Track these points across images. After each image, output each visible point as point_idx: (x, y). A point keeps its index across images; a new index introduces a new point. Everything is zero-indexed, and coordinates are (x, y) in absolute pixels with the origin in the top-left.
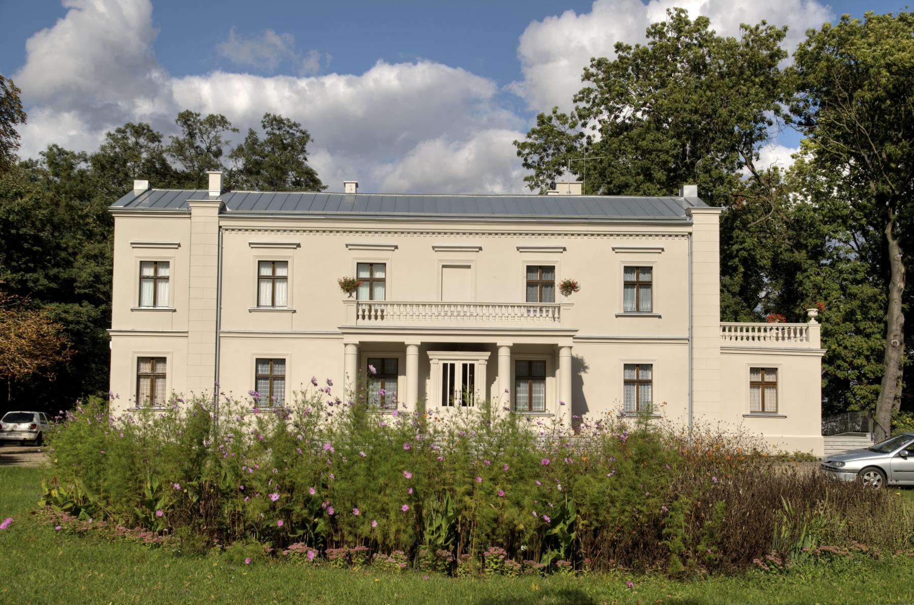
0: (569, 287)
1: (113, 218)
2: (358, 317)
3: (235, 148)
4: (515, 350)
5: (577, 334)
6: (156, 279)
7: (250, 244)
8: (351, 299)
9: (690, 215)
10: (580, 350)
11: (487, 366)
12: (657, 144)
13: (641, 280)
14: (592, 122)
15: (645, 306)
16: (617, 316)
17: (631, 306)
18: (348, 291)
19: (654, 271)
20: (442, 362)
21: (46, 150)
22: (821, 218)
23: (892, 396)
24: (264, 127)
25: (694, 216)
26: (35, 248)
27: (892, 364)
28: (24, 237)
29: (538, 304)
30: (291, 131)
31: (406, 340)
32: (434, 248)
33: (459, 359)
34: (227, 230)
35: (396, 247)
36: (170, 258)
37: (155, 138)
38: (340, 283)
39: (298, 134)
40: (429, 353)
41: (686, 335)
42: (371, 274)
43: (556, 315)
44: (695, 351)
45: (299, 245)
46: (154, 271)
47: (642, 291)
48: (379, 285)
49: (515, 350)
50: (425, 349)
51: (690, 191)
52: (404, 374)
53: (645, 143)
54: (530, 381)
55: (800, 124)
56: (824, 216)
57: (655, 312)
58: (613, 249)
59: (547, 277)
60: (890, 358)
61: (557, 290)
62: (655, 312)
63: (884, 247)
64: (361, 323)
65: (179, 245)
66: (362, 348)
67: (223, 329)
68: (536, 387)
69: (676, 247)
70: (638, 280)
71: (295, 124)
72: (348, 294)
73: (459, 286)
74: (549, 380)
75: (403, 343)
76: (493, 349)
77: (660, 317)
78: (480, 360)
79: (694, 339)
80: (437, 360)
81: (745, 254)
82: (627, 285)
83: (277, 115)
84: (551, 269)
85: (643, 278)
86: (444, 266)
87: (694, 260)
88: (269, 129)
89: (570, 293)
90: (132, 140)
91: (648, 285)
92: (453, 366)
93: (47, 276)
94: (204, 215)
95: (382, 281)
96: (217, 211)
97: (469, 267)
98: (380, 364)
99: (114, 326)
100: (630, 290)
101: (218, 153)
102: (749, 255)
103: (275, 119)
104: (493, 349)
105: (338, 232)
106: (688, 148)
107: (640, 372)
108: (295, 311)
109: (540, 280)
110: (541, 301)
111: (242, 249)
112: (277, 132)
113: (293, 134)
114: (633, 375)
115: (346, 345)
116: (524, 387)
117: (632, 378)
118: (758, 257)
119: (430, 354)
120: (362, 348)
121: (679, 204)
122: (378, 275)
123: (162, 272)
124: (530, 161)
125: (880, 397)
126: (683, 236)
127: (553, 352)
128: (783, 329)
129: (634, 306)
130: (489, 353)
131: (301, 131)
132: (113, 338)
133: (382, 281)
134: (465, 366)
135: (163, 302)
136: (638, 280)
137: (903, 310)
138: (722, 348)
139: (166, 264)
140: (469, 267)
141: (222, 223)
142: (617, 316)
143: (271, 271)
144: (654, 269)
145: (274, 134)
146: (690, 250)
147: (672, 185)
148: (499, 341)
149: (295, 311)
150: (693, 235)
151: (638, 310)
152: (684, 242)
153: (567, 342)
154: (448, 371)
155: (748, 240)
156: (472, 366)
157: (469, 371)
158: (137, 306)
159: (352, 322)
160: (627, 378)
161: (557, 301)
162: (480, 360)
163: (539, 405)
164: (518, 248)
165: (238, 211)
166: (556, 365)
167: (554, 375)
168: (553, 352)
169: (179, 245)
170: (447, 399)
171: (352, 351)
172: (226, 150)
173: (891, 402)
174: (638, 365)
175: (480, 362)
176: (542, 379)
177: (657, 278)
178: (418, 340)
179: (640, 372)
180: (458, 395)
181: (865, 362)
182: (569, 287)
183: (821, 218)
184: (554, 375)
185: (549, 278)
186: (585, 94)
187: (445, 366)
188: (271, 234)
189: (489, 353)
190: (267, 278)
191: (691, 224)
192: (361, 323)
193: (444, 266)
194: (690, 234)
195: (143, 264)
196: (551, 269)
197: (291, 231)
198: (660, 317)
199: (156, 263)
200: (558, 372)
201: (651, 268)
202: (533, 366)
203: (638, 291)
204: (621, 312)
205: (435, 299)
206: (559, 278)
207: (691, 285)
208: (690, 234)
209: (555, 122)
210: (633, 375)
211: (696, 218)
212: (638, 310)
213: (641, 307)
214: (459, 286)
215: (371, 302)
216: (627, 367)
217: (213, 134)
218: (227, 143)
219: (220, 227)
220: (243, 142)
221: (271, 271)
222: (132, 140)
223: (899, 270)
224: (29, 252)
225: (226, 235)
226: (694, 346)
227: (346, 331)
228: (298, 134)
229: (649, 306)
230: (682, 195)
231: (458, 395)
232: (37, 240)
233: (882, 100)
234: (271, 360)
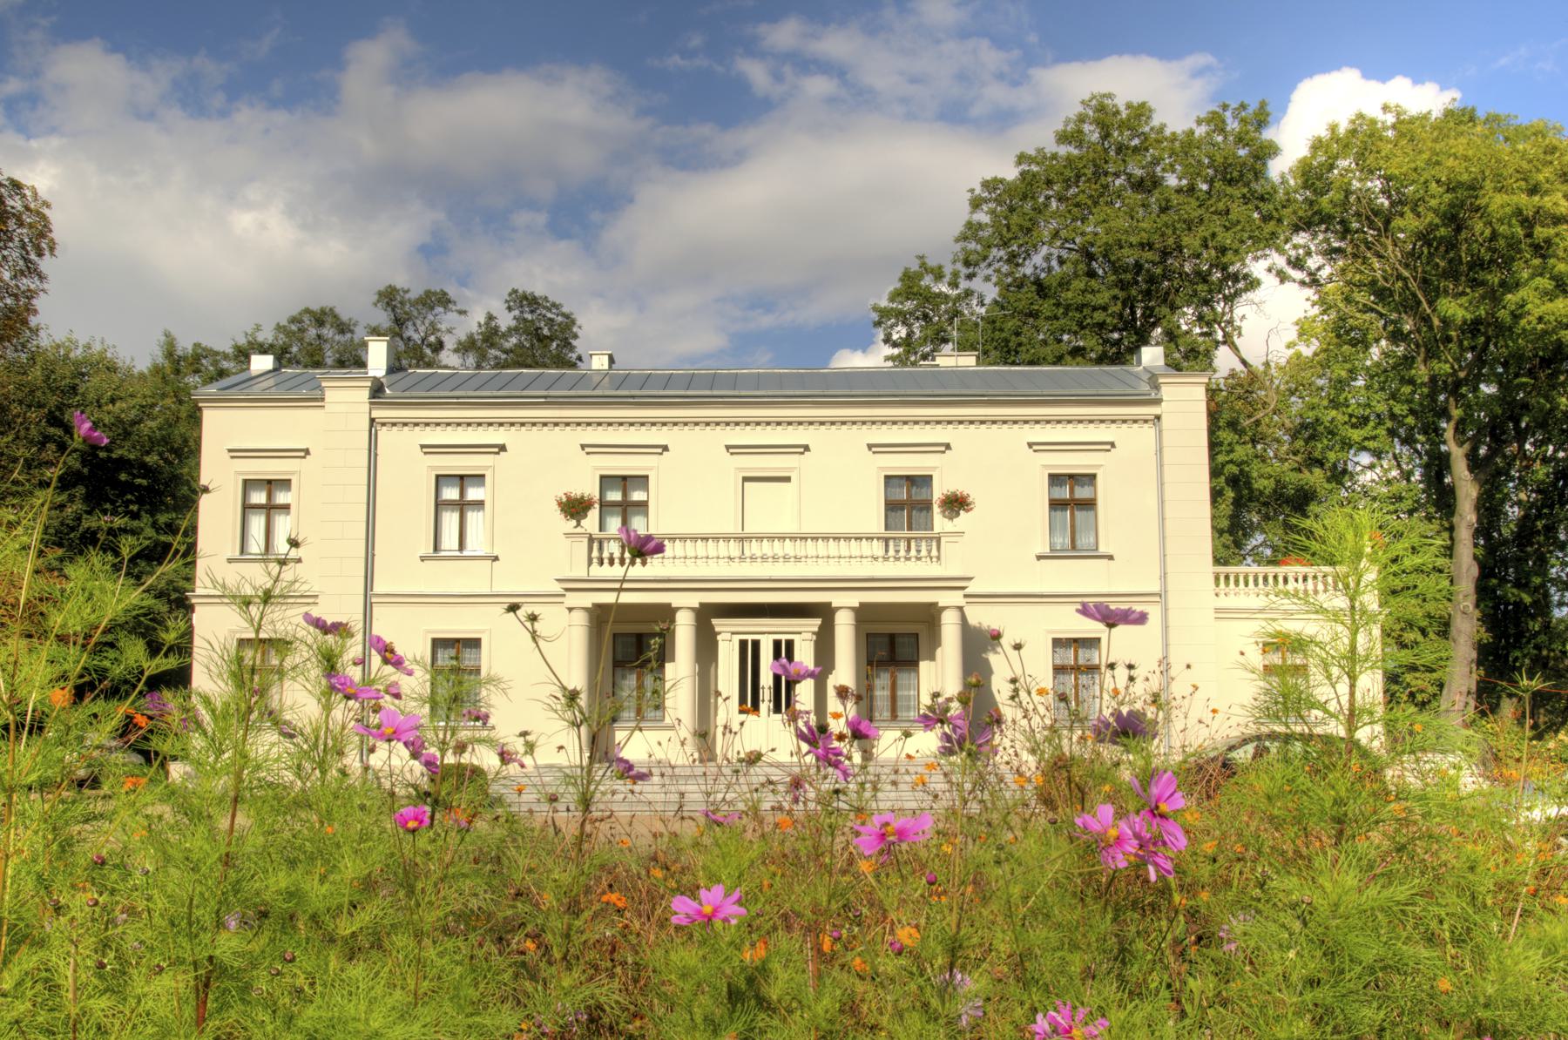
0: (956, 504)
1: (200, 409)
2: (590, 562)
3: (463, 338)
4: (864, 614)
5: (973, 588)
6: (462, 506)
7: (422, 446)
8: (579, 530)
9: (1157, 387)
10: (981, 616)
11: (817, 644)
12: (1089, 296)
13: (1077, 496)
14: (983, 271)
15: (1084, 540)
16: (1039, 558)
17: (1063, 540)
18: (572, 517)
19: (1100, 480)
20: (737, 638)
21: (185, 345)
22: (1346, 418)
23: (1464, 689)
24: (510, 309)
25: (1164, 389)
26: (138, 481)
27: (1462, 640)
28: (123, 463)
29: (906, 533)
30: (549, 315)
31: (674, 599)
32: (728, 447)
33: (766, 632)
34: (383, 424)
35: (665, 448)
36: (292, 473)
37: (343, 328)
38: (560, 503)
39: (560, 319)
40: (714, 621)
41: (1156, 588)
42: (625, 494)
43: (934, 553)
44: (1170, 613)
45: (503, 448)
46: (265, 497)
47: (1079, 515)
48: (638, 513)
49: (864, 614)
50: (706, 615)
51: (1152, 355)
52: (673, 660)
53: (1070, 295)
54: (892, 668)
55: (1302, 283)
56: (1351, 416)
57: (1103, 549)
58: (1030, 445)
59: (918, 494)
60: (1459, 632)
61: (936, 509)
62: (1103, 549)
63: (1437, 466)
64: (597, 571)
65: (307, 452)
66: (599, 616)
67: (379, 587)
68: (903, 678)
69: (1134, 440)
70: (1072, 498)
71: (554, 305)
72: (574, 522)
73: (771, 510)
74: (924, 666)
75: (669, 605)
76: (825, 613)
77: (1111, 558)
78: (803, 634)
79: (1171, 595)
80: (729, 637)
81: (1235, 469)
82: (1056, 505)
83: (529, 291)
84: (927, 480)
85: (1082, 493)
86: (745, 479)
87: (1166, 460)
88: (517, 313)
89: (958, 514)
90: (312, 332)
91: (1089, 505)
92: (756, 644)
93: (154, 525)
94: (346, 399)
95: (643, 506)
96: (366, 393)
97: (787, 479)
98: (629, 646)
99: (199, 591)
100: (1059, 513)
101: (439, 347)
102: (1241, 471)
103: (525, 297)
104: (825, 613)
105: (567, 424)
106: (1139, 313)
107: (1080, 652)
108: (496, 558)
109: (909, 502)
110: (910, 529)
111: (410, 454)
112: (529, 317)
113: (551, 320)
114: (1068, 657)
115: (570, 609)
116: (882, 682)
117: (1066, 662)
118: (1255, 474)
119: (718, 623)
120: (599, 616)
121: (1137, 376)
122: (637, 496)
123: (473, 494)
124: (895, 337)
125: (1445, 692)
126: (1146, 421)
127: (930, 616)
128: (1315, 577)
129: (1068, 541)
130: (818, 621)
131: (564, 315)
132: (197, 608)
133: (643, 506)
134: (777, 644)
135: (475, 544)
136: (1072, 498)
137: (1475, 557)
138: (1217, 610)
139: (479, 479)
140: (787, 479)
141: (375, 414)
142: (1039, 558)
143: (456, 494)
144: (1099, 478)
145: (525, 320)
146: (1154, 452)
147: (1120, 355)
148: (836, 599)
149: (496, 558)
150: (1164, 418)
151: (1074, 547)
152: (1148, 431)
153: (955, 598)
154: (749, 653)
155: (1238, 448)
156: (790, 644)
157: (783, 650)
158: (237, 554)
159: (580, 571)
160: (1058, 662)
161: (937, 529)
162: (803, 634)
163: (908, 709)
164: (870, 446)
165: (407, 394)
166: (935, 640)
167: (932, 658)
168: (930, 616)
169: (307, 452)
170: (750, 701)
171: (580, 619)
172: (450, 342)
173: (1463, 699)
174: (1076, 640)
175: (805, 636)
176: (913, 664)
177: (1105, 492)
178: (695, 600)
179: (1080, 652)
180: (766, 694)
181: (1420, 638)
182: (956, 504)
183: (1346, 418)
184: (932, 658)
185: (923, 497)
186: (972, 230)
187: (743, 644)
188: (460, 430)
189: (818, 621)
190: (450, 504)
191: (1158, 402)
192: (597, 571)
193: (745, 479)
194: (1158, 418)
195: (440, 480)
196: (927, 480)
197: (480, 424)
198: (1111, 558)
199: (269, 482)
200: (939, 651)
201: (1093, 476)
202: (895, 641)
203: (1072, 515)
204: (1046, 550)
205: (732, 528)
206: (938, 492)
207: (1162, 502)
208: (1158, 418)
209: (927, 281)
210: (1068, 657)
211: (1166, 392)
212: (1074, 547)
213: (1078, 543)
214: (771, 510)
215: (602, 535)
216: (1058, 643)
217: (430, 317)
218: (449, 331)
219: (372, 420)
220: (475, 329)
221: (456, 494)
222: (312, 332)
223: (1467, 495)
224: (129, 487)
225: (384, 434)
226: (1171, 605)
227: (572, 585)
228: (560, 319)
229: (1092, 540)
230: (1139, 363)
231: (766, 694)
232: (146, 470)
233: (1432, 228)
234: (457, 640)
